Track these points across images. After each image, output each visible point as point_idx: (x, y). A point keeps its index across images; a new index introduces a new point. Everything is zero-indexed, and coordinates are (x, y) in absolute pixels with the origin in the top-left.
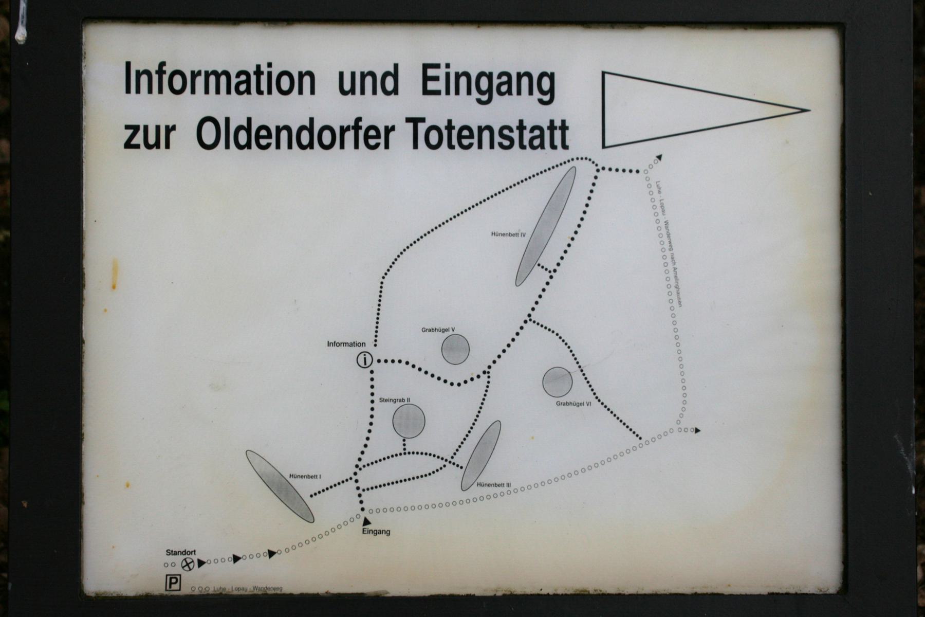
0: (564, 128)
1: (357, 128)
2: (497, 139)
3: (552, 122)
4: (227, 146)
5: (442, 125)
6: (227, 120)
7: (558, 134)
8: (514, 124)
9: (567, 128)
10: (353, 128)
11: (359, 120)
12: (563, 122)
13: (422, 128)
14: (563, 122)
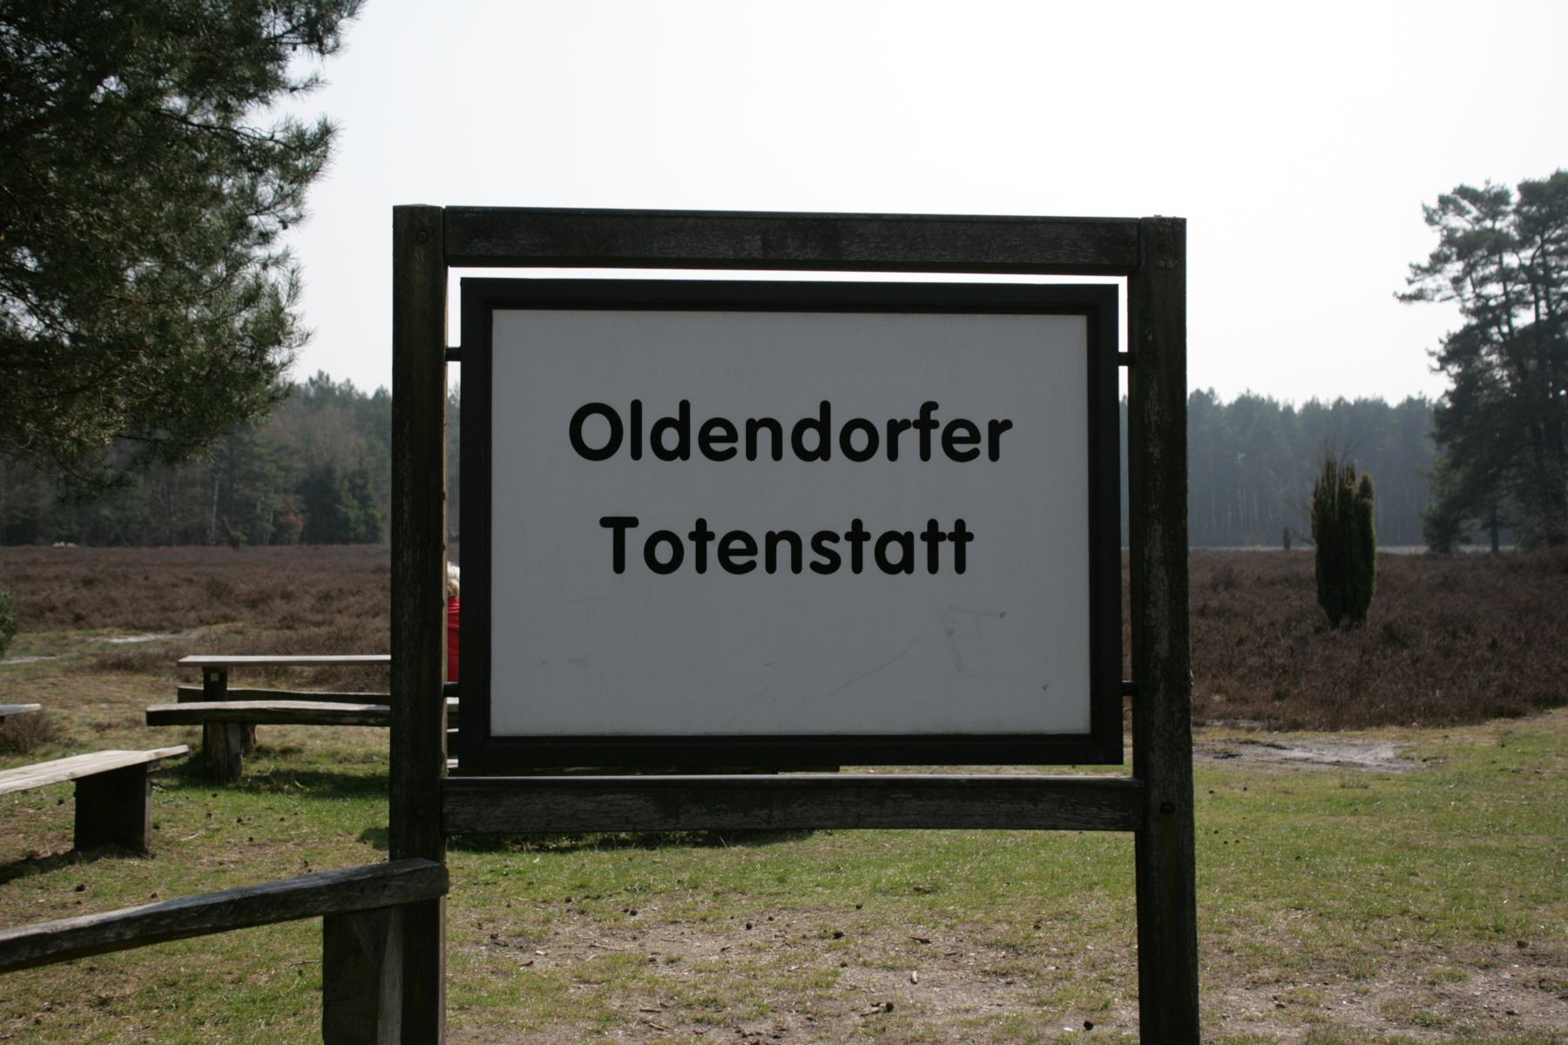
0: (961, 536)
1: (925, 423)
2: (809, 555)
3: (933, 524)
4: (636, 453)
5: (683, 530)
6: (636, 407)
7: (947, 549)
8: (842, 528)
9: (970, 537)
10: (917, 424)
11: (929, 407)
12: (960, 524)
13: (635, 540)
14: (960, 524)
